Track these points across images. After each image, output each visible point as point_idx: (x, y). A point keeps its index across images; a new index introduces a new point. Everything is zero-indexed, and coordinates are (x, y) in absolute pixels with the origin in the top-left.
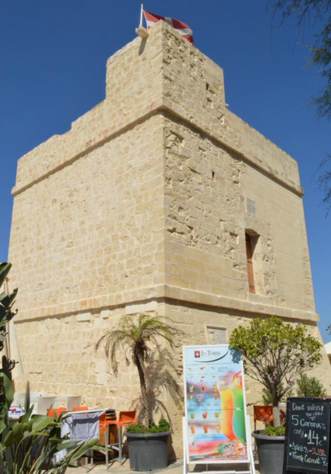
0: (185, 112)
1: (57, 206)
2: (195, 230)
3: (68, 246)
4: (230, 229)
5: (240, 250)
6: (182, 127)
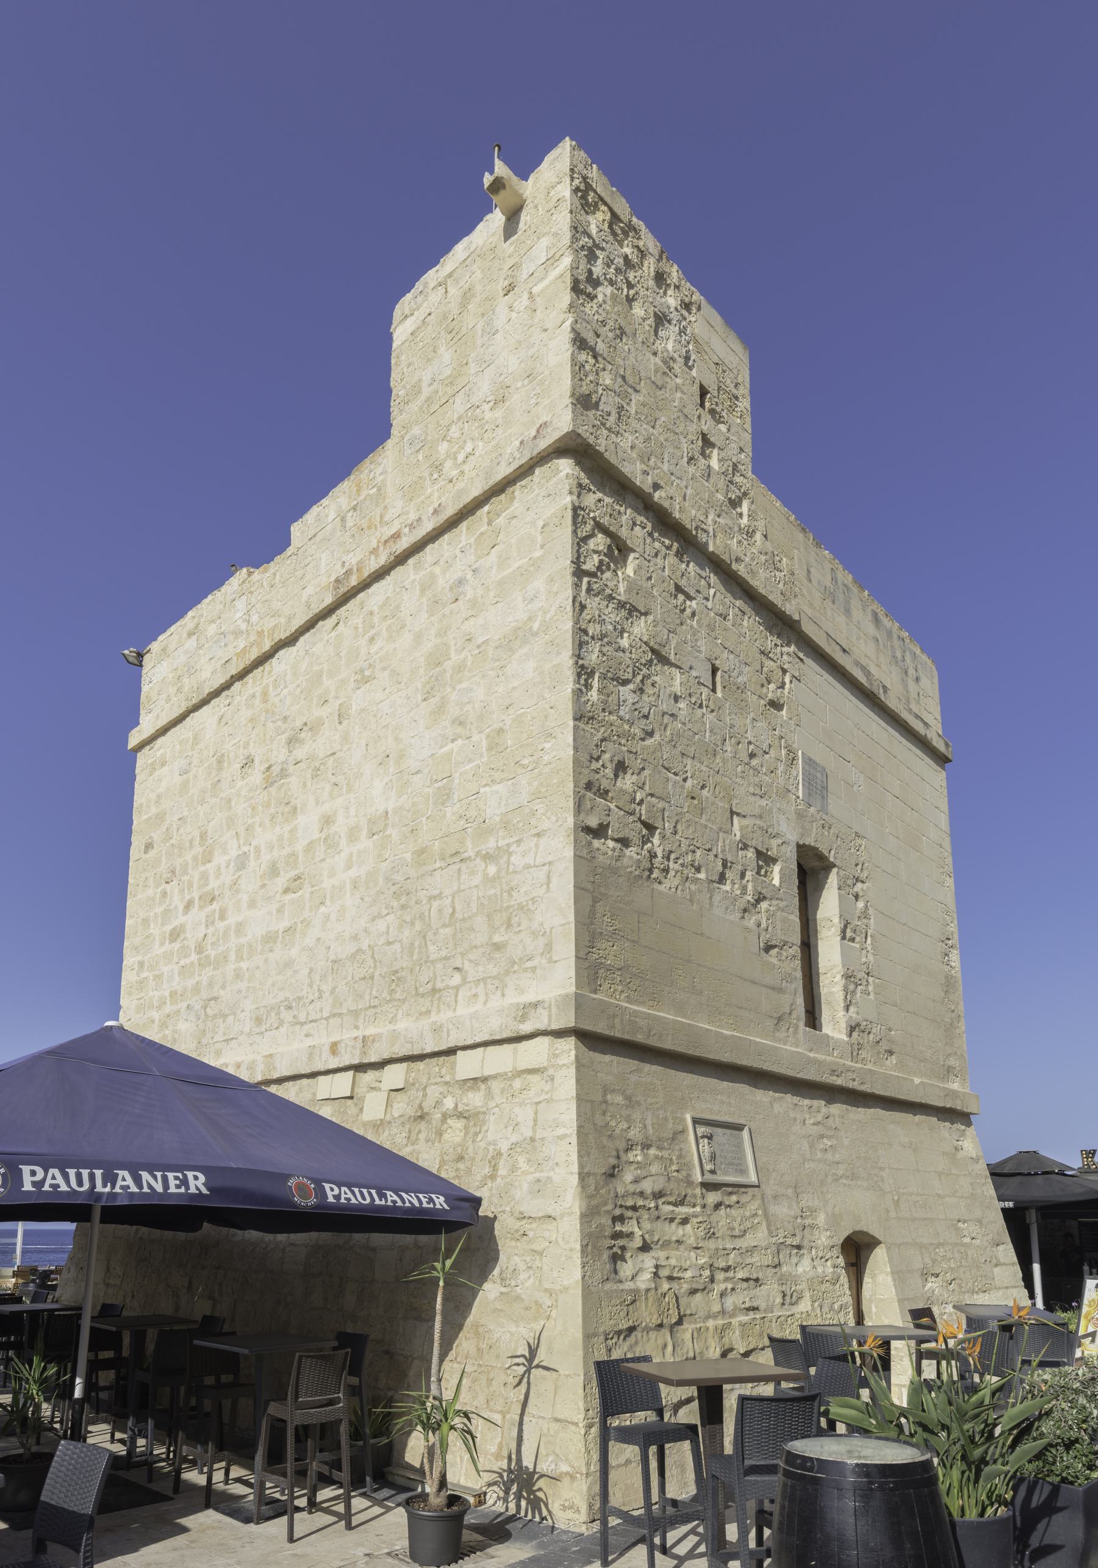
0: (639, 466)
1: (256, 776)
2: (663, 837)
3: (286, 891)
4: (756, 841)
5: (782, 904)
6: (628, 514)
